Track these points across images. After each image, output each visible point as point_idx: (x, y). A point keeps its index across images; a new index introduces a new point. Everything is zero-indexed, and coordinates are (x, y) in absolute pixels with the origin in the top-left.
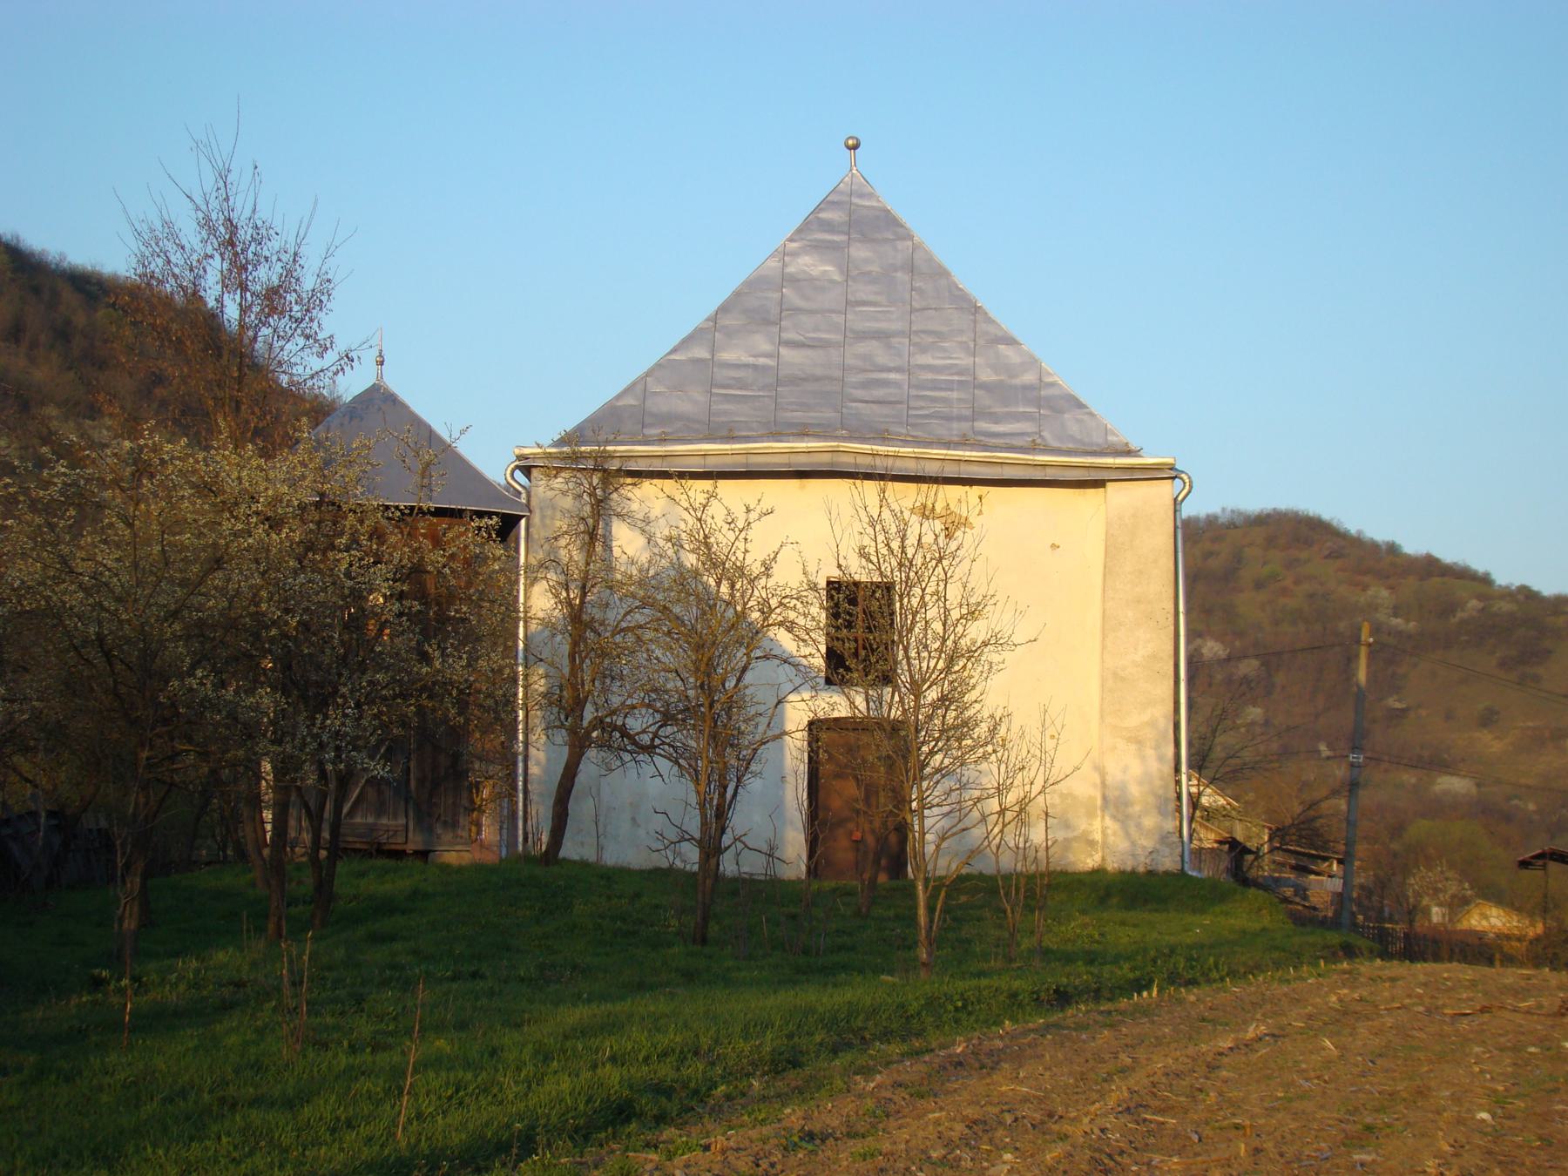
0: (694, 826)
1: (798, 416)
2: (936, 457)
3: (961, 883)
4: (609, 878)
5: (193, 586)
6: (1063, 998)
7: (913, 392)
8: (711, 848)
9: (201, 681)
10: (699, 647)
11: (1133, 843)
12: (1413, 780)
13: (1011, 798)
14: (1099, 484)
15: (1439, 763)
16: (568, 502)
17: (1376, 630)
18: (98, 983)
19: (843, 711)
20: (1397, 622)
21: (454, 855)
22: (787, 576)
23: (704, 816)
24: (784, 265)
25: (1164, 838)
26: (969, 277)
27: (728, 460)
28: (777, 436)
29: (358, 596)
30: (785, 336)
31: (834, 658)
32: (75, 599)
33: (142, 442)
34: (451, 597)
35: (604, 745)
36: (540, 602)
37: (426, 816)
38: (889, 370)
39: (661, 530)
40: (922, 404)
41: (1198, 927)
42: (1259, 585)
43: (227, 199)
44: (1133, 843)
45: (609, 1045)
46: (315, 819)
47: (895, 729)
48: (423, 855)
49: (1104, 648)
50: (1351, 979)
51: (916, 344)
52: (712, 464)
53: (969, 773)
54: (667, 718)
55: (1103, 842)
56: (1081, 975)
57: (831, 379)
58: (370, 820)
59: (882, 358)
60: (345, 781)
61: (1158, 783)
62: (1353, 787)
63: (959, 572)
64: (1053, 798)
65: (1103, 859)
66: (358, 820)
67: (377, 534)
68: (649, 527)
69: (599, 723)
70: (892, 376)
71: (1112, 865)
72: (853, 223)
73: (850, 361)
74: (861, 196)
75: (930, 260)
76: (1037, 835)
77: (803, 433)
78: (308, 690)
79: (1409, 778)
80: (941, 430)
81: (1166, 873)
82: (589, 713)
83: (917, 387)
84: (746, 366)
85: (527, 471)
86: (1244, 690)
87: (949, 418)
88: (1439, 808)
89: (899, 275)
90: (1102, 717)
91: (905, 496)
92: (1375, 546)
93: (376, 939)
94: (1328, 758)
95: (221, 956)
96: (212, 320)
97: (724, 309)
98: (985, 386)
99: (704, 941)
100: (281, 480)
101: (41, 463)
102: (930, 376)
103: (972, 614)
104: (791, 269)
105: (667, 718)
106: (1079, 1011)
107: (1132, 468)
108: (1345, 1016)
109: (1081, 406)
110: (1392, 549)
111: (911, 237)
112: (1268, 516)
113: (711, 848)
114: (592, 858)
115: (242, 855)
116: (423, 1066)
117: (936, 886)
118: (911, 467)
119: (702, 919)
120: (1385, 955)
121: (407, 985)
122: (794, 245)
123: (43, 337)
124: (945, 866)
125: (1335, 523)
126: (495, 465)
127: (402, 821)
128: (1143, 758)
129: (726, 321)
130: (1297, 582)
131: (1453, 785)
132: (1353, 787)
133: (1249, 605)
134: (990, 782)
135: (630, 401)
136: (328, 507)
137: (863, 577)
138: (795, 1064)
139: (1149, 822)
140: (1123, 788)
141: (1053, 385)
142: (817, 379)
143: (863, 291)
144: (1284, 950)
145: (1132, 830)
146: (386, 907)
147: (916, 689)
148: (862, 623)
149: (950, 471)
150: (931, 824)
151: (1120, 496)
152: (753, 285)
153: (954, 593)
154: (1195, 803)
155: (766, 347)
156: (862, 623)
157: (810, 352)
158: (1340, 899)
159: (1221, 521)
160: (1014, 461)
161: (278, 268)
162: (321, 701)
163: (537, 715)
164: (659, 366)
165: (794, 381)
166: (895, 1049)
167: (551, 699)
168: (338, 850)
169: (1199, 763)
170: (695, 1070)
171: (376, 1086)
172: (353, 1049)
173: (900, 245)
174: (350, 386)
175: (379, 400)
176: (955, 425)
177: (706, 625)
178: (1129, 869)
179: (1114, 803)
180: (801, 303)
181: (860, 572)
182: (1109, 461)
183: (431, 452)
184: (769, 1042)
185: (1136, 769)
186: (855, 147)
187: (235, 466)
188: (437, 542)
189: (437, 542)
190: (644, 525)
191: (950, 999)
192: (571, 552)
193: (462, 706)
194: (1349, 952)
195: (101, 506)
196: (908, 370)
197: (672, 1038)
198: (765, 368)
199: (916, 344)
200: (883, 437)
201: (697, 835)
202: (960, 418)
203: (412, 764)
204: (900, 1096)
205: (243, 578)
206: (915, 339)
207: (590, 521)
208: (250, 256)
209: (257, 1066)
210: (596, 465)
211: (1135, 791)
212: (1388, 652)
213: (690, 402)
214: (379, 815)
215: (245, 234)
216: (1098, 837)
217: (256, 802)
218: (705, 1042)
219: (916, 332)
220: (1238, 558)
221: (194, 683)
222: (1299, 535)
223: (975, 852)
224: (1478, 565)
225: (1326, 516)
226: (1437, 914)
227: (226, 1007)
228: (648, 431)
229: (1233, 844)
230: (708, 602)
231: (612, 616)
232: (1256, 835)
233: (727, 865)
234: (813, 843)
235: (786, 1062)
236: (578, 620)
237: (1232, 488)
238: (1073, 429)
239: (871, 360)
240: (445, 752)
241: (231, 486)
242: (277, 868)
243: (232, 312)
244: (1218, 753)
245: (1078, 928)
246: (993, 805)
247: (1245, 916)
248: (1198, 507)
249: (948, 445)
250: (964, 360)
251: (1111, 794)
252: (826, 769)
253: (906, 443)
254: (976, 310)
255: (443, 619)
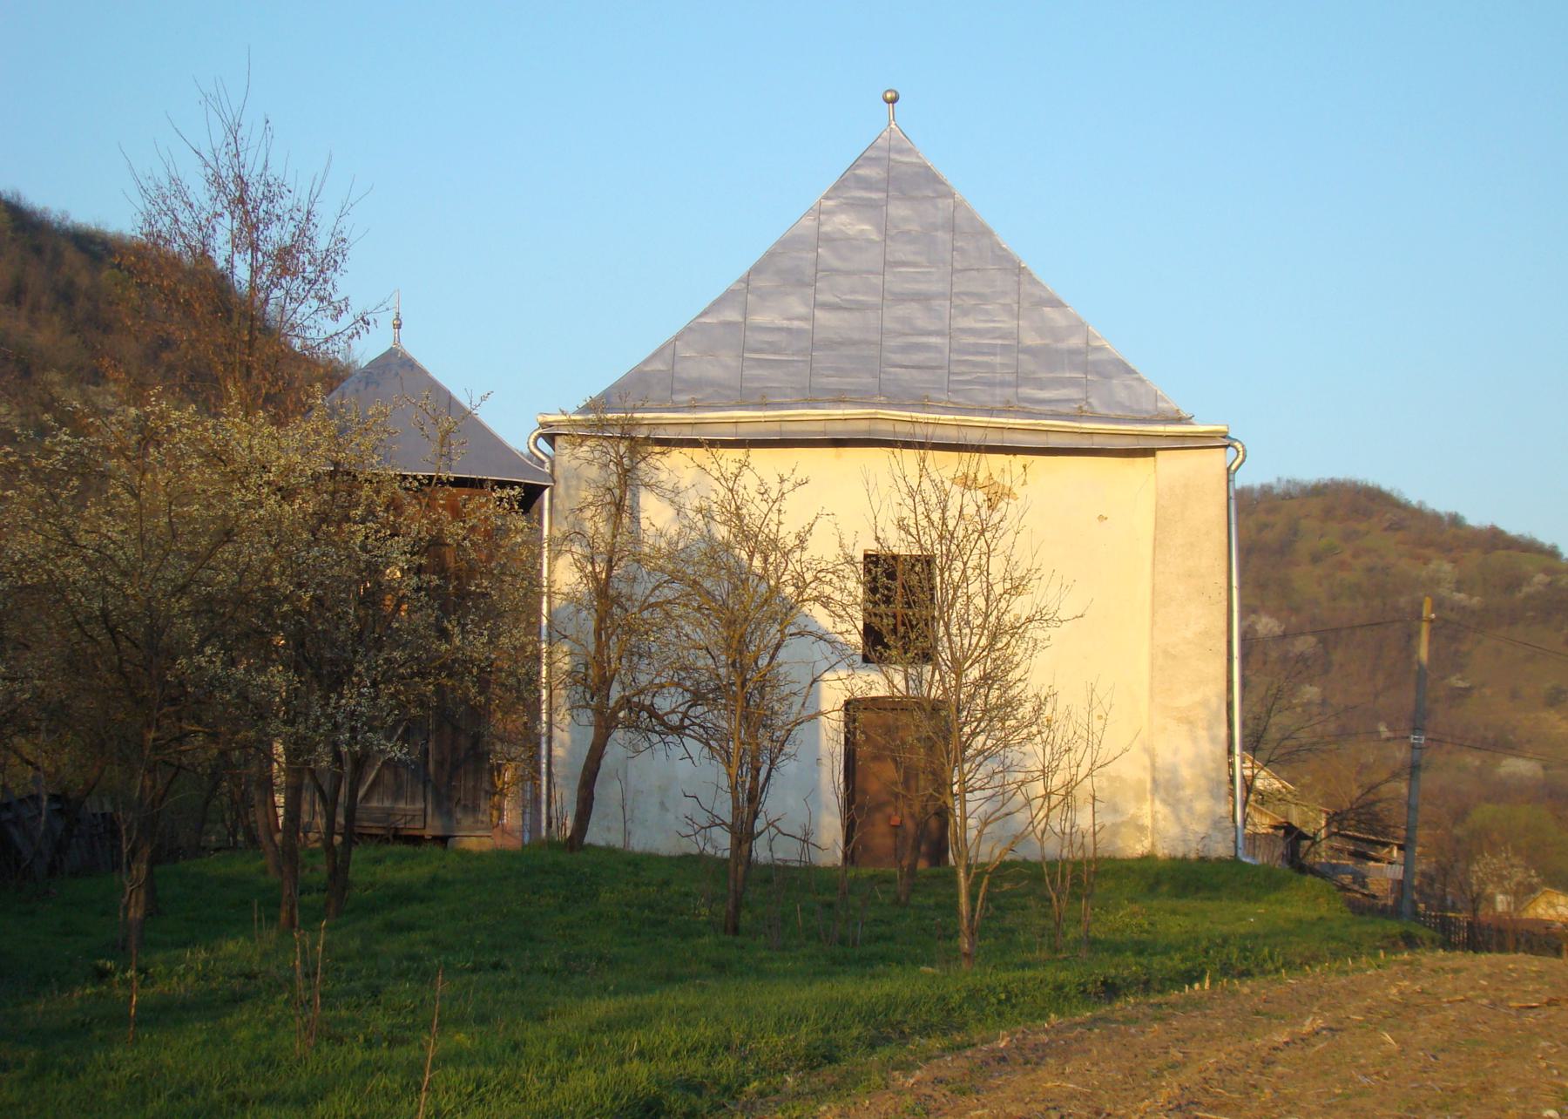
0: (725, 810)
1: (834, 382)
2: (978, 424)
3: (1004, 870)
4: (637, 864)
5: (201, 560)
6: (1111, 990)
7: (954, 357)
8: (743, 834)
9: (210, 659)
10: (730, 623)
11: (1185, 829)
12: (1477, 763)
13: (1057, 781)
14: (1149, 453)
15: (1504, 745)
16: (593, 472)
17: (1438, 605)
18: (102, 975)
19: (881, 690)
20: (1460, 597)
21: (474, 840)
22: (823, 549)
23: (735, 799)
24: (820, 224)
25: (1216, 823)
26: (1012, 236)
27: (762, 427)
28: (811, 402)
29: (374, 570)
30: (821, 298)
31: (872, 635)
32: (79, 573)
33: (148, 409)
34: (472, 571)
35: (632, 726)
36: (564, 576)
37: (445, 801)
38: (930, 333)
39: (691, 501)
40: (964, 369)
41: (1253, 915)
42: (1316, 559)
43: (237, 155)
44: (1185, 829)
45: (637, 1039)
46: (330, 802)
47: (935, 708)
48: (442, 840)
49: (1153, 623)
50: (1413, 971)
51: (957, 307)
52: (745, 432)
53: (1013, 755)
54: (697, 698)
55: (1153, 827)
56: (1131, 966)
57: (868, 343)
58: (387, 804)
59: (922, 321)
60: (360, 763)
61: (1210, 765)
62: (1414, 769)
63: (1002, 545)
64: (1100, 781)
65: (1153, 845)
66: (374, 804)
67: (394, 505)
68: (680, 497)
69: (626, 702)
70: (933, 340)
71: (1162, 851)
72: (891, 180)
73: (888, 325)
74: (900, 151)
75: (972, 218)
76: (1084, 820)
77: (839, 399)
78: (322, 668)
79: (1472, 760)
80: (983, 396)
81: (1219, 860)
82: (616, 692)
83: (959, 351)
84: (780, 329)
85: (551, 439)
86: (1300, 669)
87: (991, 384)
88: (1503, 792)
89: (940, 234)
90: (1152, 697)
91: (946, 465)
92: (1436, 518)
93: (393, 928)
94: (1388, 739)
95: (231, 947)
96: (220, 283)
97: (757, 270)
98: (1029, 351)
99: (736, 931)
100: (295, 448)
101: (43, 431)
102: (972, 340)
103: (1016, 589)
104: (826, 228)
105: (697, 698)
106: (1127, 1004)
107: (1183, 436)
108: (1405, 1010)
109: (1130, 371)
110: (1455, 520)
111: (952, 195)
112: (1326, 486)
113: (743, 834)
114: (619, 844)
115: (253, 840)
116: (442, 1061)
117: (978, 873)
118: (952, 435)
119: (734, 907)
120: (1448, 945)
121: (426, 977)
122: (830, 203)
123: (44, 300)
124: (988, 852)
125: (1395, 494)
126: (515, 430)
127: (419, 805)
128: (1194, 740)
129: (761, 282)
130: (1356, 555)
131: (1518, 767)
132: (1414, 769)
133: (1305, 579)
134: (1035, 764)
135: (658, 366)
136: (343, 477)
137: (903, 551)
138: (831, 1059)
139: (1201, 806)
140: (1173, 770)
141: (1100, 349)
142: (854, 343)
143: (902, 251)
144: (1342, 940)
145: (1184, 815)
146: (403, 895)
147: (958, 667)
148: (900, 599)
149: (994, 439)
150: (972, 810)
151: (1169, 464)
152: (787, 244)
153: (997, 567)
154: (1249, 787)
155: (801, 310)
156: (900, 599)
157: (846, 315)
158: (1400, 886)
159: (1275, 491)
160: (1060, 429)
161: (291, 227)
162: (337, 681)
163: (561, 695)
164: (689, 329)
165: (830, 345)
166: (936, 1043)
167: (575, 678)
168: (353, 836)
169: (1254, 743)
170: (727, 1065)
171: (393, 1082)
172: (369, 1044)
173: (941, 203)
174: (366, 350)
175: (396, 365)
176: (998, 391)
177: (738, 601)
178: (1180, 855)
179: (1165, 786)
180: (836, 263)
181: (900, 545)
182: (1160, 429)
183: (449, 418)
184: (804, 1036)
185: (1187, 751)
186: (894, 101)
187: (246, 434)
188: (457, 514)
189: (457, 514)
190: (673, 496)
191: (992, 990)
192: (597, 524)
193: (483, 684)
194: (1410, 942)
195: (105, 476)
196: (949, 333)
197: (704, 1031)
198: (800, 332)
199: (957, 307)
200: (923, 404)
201: (729, 820)
202: (1003, 384)
203: (431, 746)
204: (940, 1093)
205: (254, 551)
206: (957, 301)
207: (617, 492)
208: (262, 214)
209: (269, 1062)
210: (624, 433)
211: (1186, 773)
212: (1450, 628)
213: (719, 367)
214: (396, 799)
215: (256, 191)
216: (1147, 822)
217: (267, 785)
218: (737, 1036)
219: (958, 295)
220: (1294, 531)
221: (203, 661)
222: (1358, 505)
223: (1018, 838)
224: (1545, 538)
225: (1386, 486)
226: (1501, 902)
227: (236, 1000)
228: (677, 398)
229: (1289, 829)
230: (740, 578)
231: (640, 591)
232: (1311, 818)
233: (761, 851)
234: (849, 829)
235: (821, 1057)
236: (604, 595)
237: (1286, 459)
238: (1122, 395)
239: (910, 324)
240: (464, 735)
241: (241, 456)
242: (290, 855)
243: (242, 273)
244: (1273, 733)
245: (1127, 916)
246: (1038, 788)
247: (1301, 904)
248: (1249, 478)
249: (990, 412)
250: (1007, 323)
251: (1161, 777)
252: (863, 750)
253: (946, 410)
254: (1020, 271)
255: (463, 595)
